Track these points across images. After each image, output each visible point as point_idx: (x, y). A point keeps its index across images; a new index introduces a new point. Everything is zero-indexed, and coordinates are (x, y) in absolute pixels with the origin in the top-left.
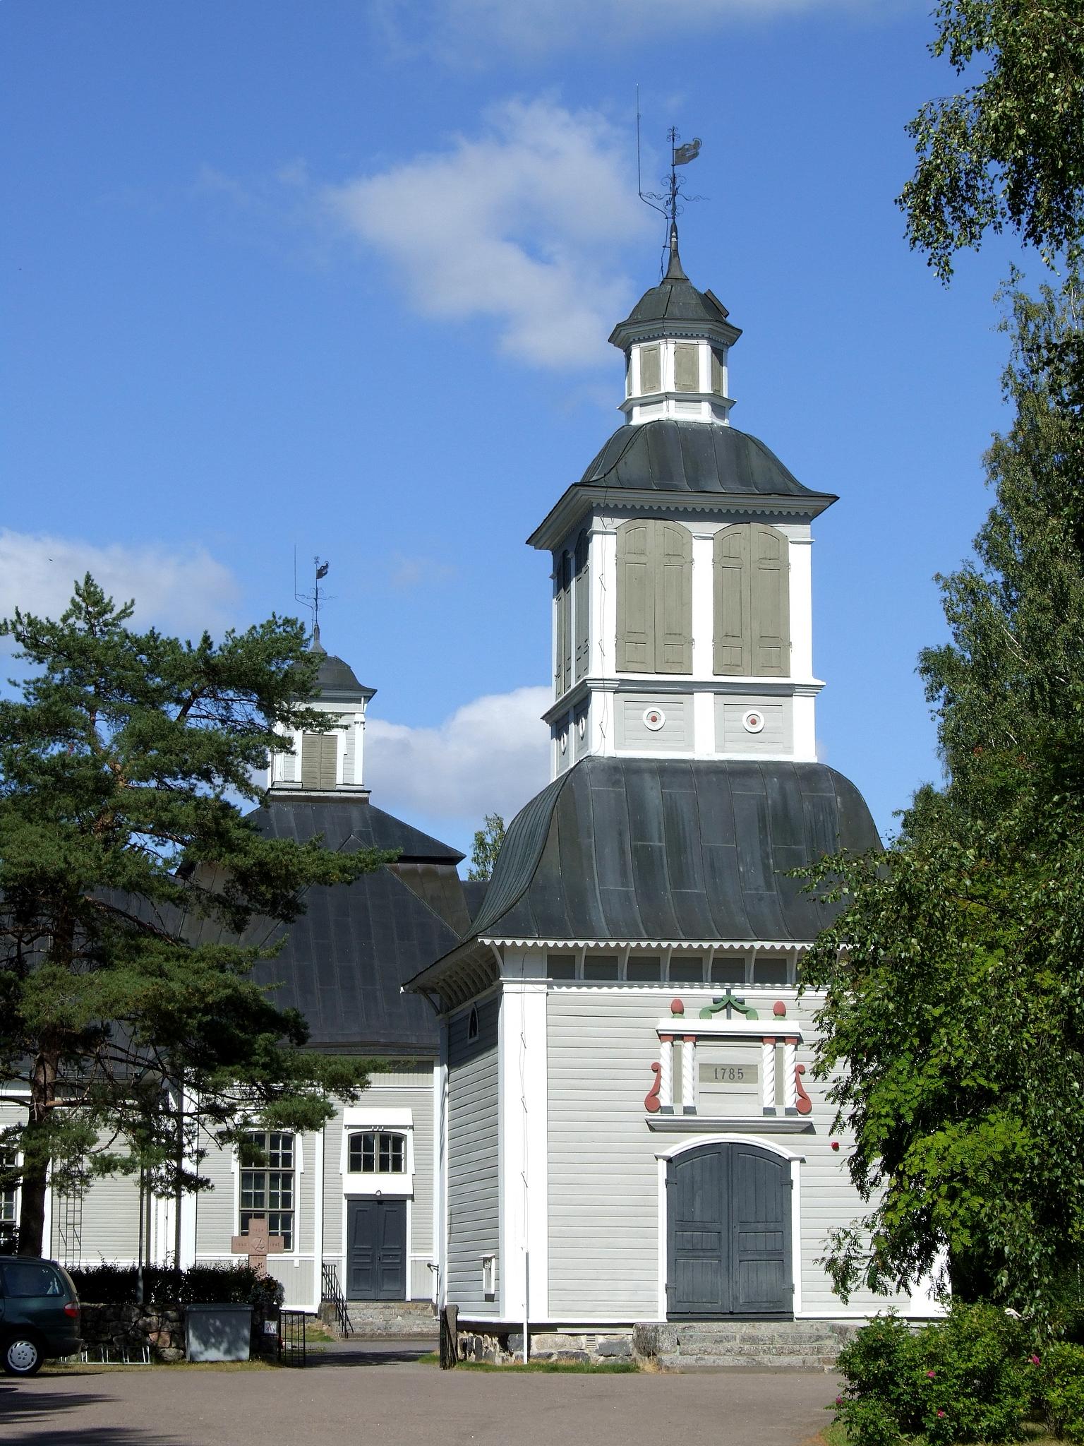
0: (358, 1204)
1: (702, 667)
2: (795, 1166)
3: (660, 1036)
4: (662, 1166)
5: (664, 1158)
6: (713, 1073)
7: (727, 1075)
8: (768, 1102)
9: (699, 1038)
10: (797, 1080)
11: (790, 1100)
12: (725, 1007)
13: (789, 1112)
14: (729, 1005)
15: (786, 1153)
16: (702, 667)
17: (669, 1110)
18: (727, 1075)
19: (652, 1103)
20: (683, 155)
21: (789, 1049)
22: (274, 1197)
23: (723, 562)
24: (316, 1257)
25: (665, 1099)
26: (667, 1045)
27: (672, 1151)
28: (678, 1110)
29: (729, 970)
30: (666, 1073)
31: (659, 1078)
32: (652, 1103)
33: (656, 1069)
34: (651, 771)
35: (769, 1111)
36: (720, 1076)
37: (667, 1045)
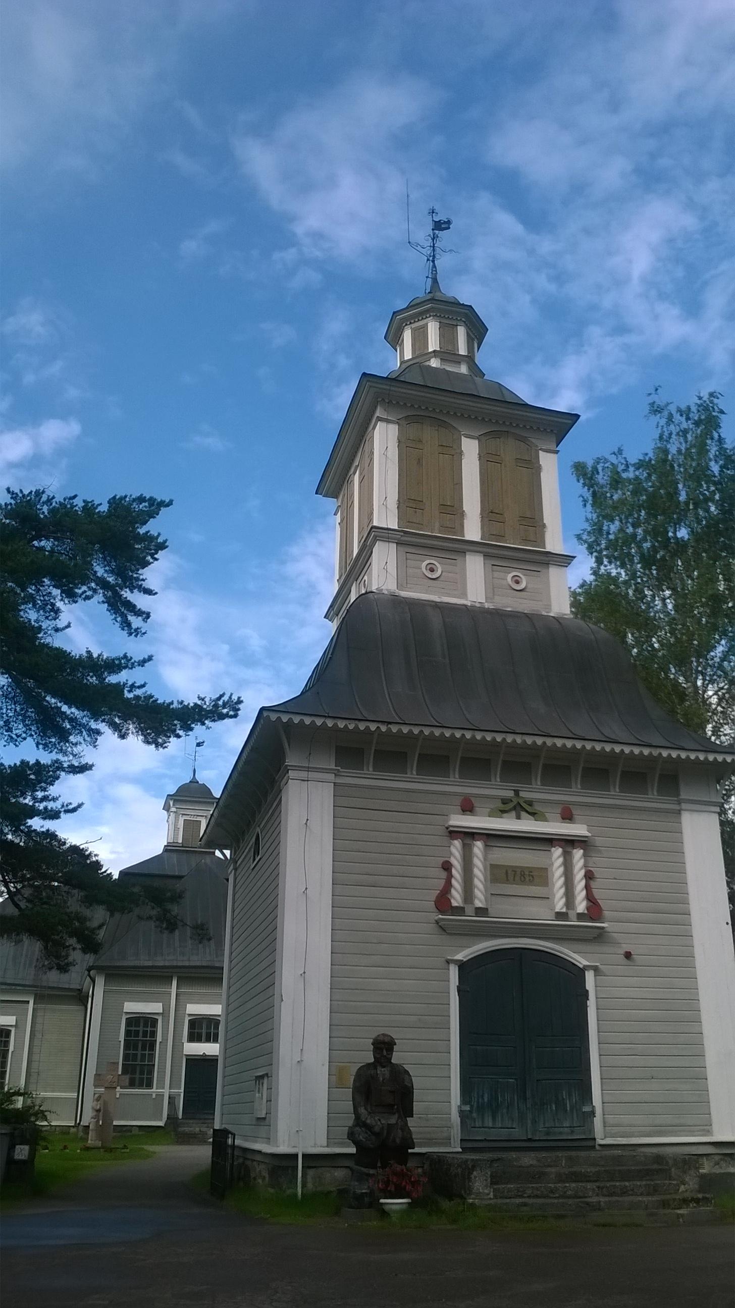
0: (297, 1155)
1: (473, 531)
2: (590, 976)
3: (451, 832)
4: (454, 973)
5: (455, 962)
6: (501, 875)
7: (517, 878)
8: (560, 905)
9: (491, 838)
10: (587, 887)
11: (581, 906)
12: (514, 808)
13: (580, 916)
14: (519, 808)
15: (581, 961)
16: (473, 531)
17: (460, 911)
18: (517, 878)
19: (443, 902)
20: (440, 226)
21: (578, 854)
22: (143, 1056)
23: (486, 458)
24: (166, 1092)
25: (457, 899)
26: (457, 843)
27: (463, 955)
28: (469, 910)
29: (519, 765)
30: (457, 873)
31: (450, 876)
32: (443, 902)
33: (447, 867)
34: (431, 606)
35: (560, 916)
36: (511, 878)
37: (457, 843)
